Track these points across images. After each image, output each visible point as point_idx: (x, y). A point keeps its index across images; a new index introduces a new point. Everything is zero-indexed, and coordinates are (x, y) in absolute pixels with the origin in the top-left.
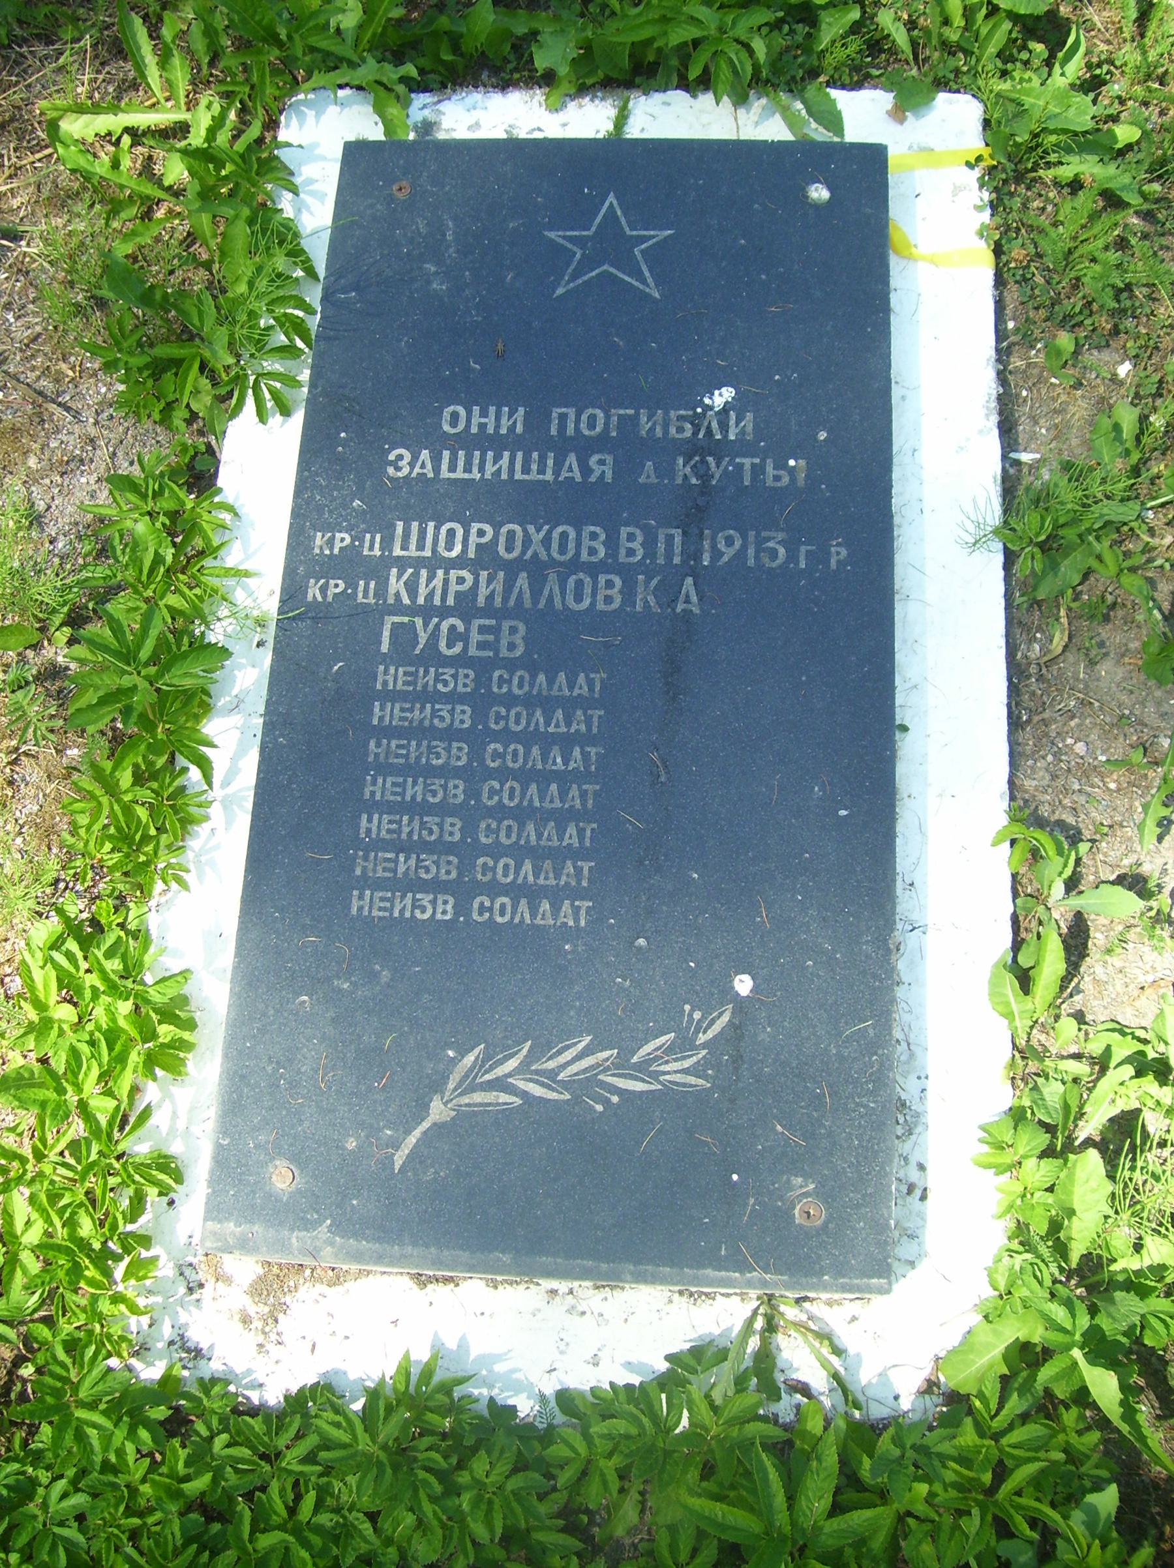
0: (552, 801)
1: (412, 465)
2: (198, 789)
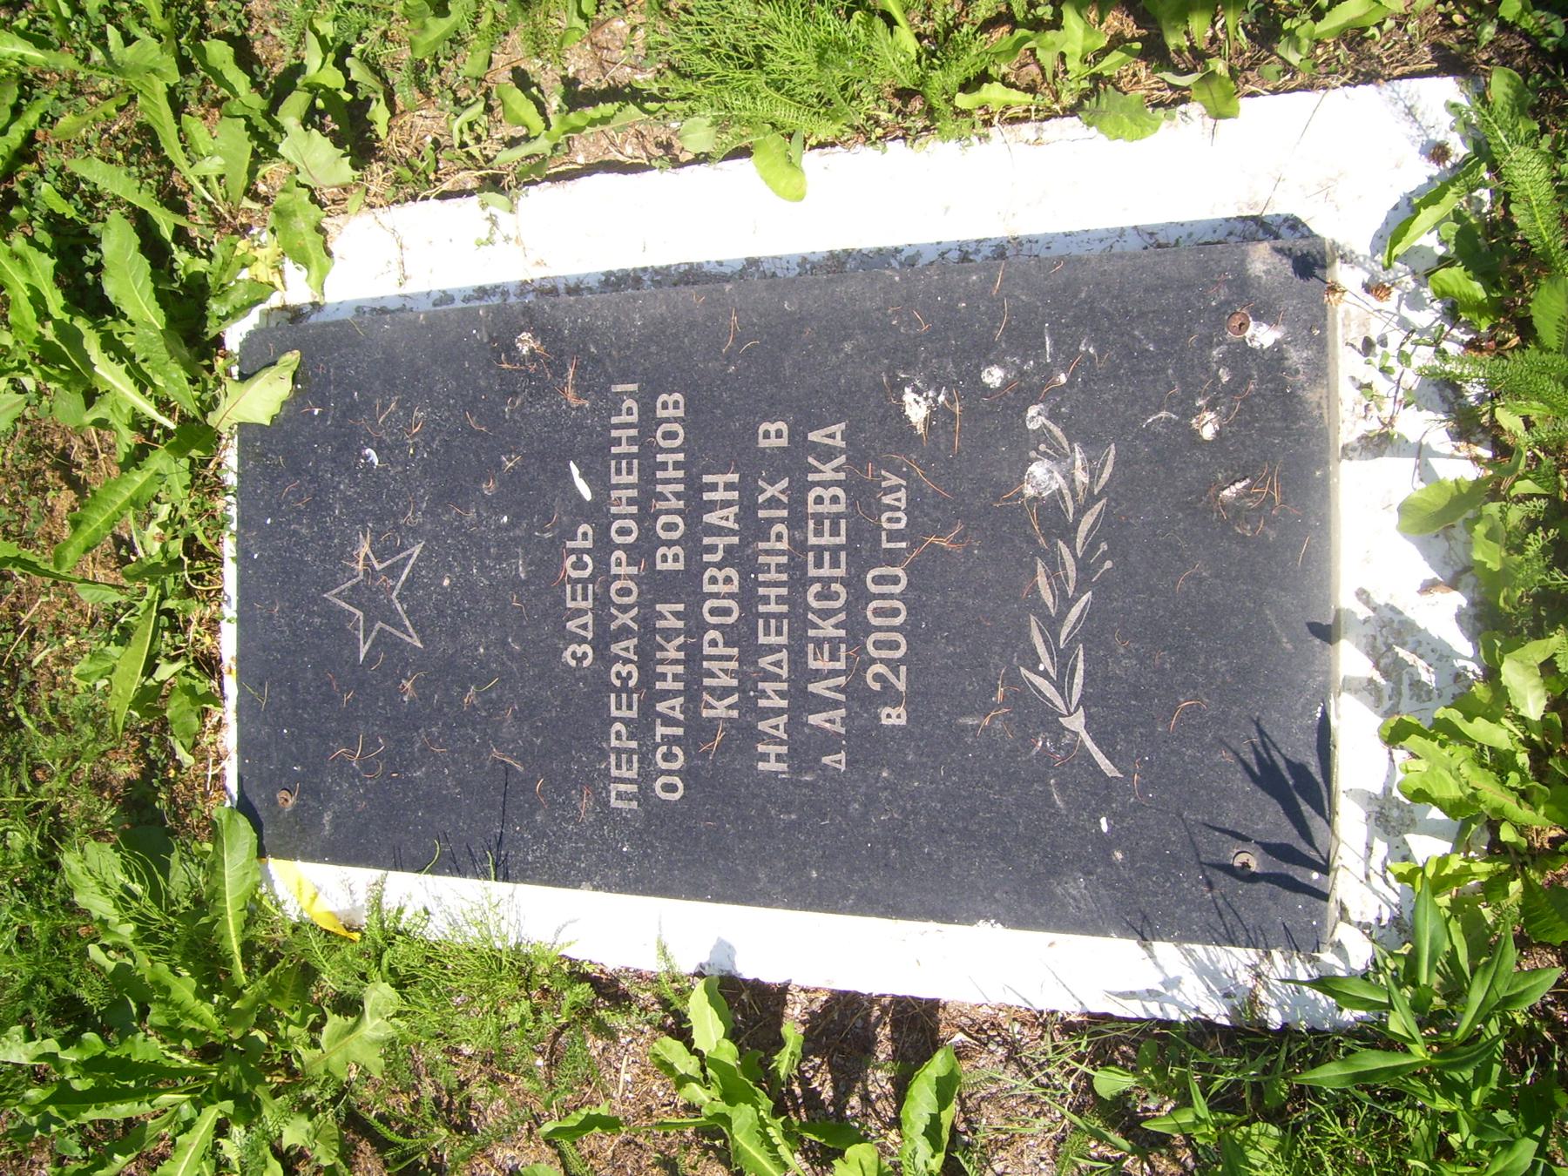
0: (899, 500)
1: (626, 661)
2: (362, 898)
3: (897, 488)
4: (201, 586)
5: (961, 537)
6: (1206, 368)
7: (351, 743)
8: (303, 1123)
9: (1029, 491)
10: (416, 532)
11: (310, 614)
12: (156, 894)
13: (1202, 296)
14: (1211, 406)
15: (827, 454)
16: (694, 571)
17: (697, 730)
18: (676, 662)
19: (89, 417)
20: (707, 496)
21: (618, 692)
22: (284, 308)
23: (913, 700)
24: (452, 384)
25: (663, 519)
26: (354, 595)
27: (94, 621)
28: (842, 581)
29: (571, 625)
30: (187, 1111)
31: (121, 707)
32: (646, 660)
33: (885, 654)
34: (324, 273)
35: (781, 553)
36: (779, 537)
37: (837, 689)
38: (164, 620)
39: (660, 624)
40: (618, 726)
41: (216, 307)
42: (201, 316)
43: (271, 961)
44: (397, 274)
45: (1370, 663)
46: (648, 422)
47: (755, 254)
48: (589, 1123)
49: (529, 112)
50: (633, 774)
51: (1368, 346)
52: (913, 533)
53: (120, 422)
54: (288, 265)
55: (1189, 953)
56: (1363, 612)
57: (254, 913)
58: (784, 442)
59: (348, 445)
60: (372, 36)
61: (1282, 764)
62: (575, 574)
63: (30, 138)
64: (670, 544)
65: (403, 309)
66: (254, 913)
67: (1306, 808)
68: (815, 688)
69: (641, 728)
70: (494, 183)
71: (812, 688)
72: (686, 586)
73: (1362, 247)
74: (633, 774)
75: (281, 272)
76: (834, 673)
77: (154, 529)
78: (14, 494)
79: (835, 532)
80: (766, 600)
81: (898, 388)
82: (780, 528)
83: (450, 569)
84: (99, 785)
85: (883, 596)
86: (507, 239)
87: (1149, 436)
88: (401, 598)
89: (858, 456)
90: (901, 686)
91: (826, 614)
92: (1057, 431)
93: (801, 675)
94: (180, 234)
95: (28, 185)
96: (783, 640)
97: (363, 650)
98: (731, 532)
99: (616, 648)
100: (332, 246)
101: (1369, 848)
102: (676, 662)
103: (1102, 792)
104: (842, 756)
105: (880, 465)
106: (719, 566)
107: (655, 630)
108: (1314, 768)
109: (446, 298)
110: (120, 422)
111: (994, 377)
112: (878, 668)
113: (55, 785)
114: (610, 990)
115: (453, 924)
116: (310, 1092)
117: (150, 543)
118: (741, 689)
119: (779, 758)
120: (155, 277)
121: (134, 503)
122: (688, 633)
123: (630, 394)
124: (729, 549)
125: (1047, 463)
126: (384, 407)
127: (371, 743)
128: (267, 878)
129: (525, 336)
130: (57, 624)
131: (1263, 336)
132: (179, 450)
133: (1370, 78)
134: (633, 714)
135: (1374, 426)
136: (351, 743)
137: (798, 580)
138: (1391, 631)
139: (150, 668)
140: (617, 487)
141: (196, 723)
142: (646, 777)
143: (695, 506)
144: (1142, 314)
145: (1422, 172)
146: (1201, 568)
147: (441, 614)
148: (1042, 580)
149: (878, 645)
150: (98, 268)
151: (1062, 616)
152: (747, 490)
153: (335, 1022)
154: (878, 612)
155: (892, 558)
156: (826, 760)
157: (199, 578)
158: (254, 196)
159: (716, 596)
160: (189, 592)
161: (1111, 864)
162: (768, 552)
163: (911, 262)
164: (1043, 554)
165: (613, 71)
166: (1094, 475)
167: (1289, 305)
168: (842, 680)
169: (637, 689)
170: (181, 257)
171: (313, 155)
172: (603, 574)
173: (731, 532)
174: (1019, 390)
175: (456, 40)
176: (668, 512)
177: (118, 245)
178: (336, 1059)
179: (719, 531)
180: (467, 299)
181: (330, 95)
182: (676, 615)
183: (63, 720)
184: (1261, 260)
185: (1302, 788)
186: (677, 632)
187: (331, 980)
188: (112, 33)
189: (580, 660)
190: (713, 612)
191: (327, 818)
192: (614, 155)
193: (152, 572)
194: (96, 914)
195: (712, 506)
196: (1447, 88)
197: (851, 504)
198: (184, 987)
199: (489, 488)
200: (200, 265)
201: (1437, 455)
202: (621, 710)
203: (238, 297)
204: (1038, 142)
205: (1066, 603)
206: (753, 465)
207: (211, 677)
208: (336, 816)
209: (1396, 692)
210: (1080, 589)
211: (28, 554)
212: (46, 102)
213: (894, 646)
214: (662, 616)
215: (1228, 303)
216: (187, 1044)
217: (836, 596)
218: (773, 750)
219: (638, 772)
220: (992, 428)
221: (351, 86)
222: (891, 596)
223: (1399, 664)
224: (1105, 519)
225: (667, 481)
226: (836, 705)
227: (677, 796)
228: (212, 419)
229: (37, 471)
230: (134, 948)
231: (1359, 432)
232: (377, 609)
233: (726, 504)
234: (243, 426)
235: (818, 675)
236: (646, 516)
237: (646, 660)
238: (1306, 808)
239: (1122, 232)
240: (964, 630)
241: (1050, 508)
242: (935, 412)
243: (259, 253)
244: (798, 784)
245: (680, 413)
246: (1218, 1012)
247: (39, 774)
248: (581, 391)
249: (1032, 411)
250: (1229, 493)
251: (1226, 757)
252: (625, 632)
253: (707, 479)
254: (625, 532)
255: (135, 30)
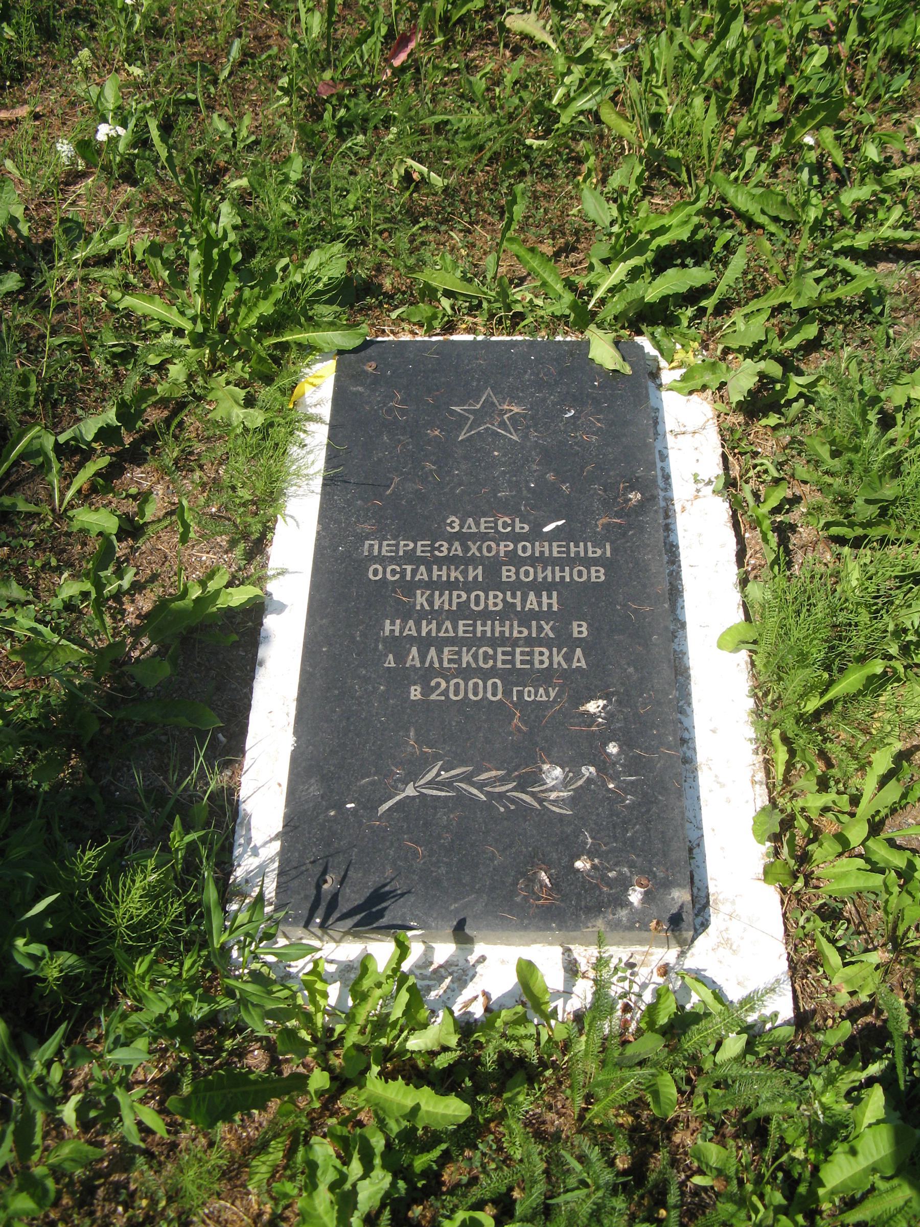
1: (449, 550)
3: (548, 695)
4: (495, 322)
5: (519, 730)
6: (616, 864)
7: (403, 402)
8: (182, 379)
9: (546, 767)
10: (525, 437)
11: (479, 380)
12: (318, 293)
13: (659, 863)
14: (594, 867)
15: (568, 658)
16: (501, 586)
17: (410, 588)
18: (449, 576)
19: (595, 261)
20: (544, 593)
21: (431, 546)
22: (659, 369)
23: (425, 705)
24: (611, 456)
25: (531, 570)
26: (489, 404)
27: (476, 266)
28: (494, 666)
29: (470, 520)
30: (190, 312)
31: (426, 276)
32: (450, 561)
33: (452, 689)
34: (679, 390)
35: (511, 633)
36: (520, 632)
37: (432, 662)
38: (476, 302)
39: (471, 568)
40: (412, 545)
41: (659, 330)
42: (653, 323)
43: (276, 360)
44: (677, 430)
45: (442, 962)
46: (588, 562)
47: (688, 626)
48: (186, 526)
49: (773, 502)
50: (384, 553)
51: (631, 966)
52: (521, 704)
53: (592, 277)
54: (683, 371)
55: (272, 860)
56: (472, 959)
57: (306, 349)
58: (575, 635)
59: (577, 400)
60: (820, 416)
61: (384, 905)
62: (500, 523)
63: (761, 226)
64: (517, 573)
65: (656, 434)
66: (306, 349)
67: (358, 917)
68: (433, 652)
69: (410, 557)
70: (731, 484)
71: (433, 649)
72: (492, 582)
73: (690, 963)
74: (384, 553)
75: (679, 367)
76: (441, 661)
77: (529, 296)
78: (550, 220)
79: (522, 662)
80: (484, 625)
81: (607, 697)
82: (526, 632)
83: (504, 455)
84: (379, 268)
85: (485, 687)
86: (698, 491)
87: (577, 833)
88: (487, 429)
89: (567, 675)
90: (433, 697)
91: (475, 657)
92: (580, 783)
93: (440, 643)
94: (702, 311)
95: (732, 226)
96: (461, 634)
97: (457, 409)
98: (523, 606)
99: (457, 544)
100: (694, 397)
101: (331, 962)
102: (449, 576)
103: (369, 804)
104: (393, 665)
105: (561, 686)
106: (504, 600)
107: (467, 565)
108: (383, 921)
109: (664, 457)
110: (592, 277)
111: (613, 749)
112: (444, 685)
113: (380, 243)
114: (258, 547)
115: (297, 460)
116: (200, 381)
117: (521, 295)
118: (432, 611)
119: (392, 631)
120: (676, 295)
121: (544, 284)
122: (466, 583)
123: (604, 553)
124: (514, 605)
125: (561, 777)
126: (599, 420)
127: (403, 412)
128: (325, 357)
129: (639, 496)
130: (473, 245)
131: (635, 896)
132: (573, 306)
133: (793, 967)
134: (419, 553)
135: (583, 967)
136: (403, 402)
137: (494, 642)
138: (461, 974)
139: (448, 294)
140: (550, 546)
141: (415, 320)
142: (381, 560)
143: (538, 587)
144: (649, 830)
145: (734, 994)
146: (499, 859)
147: (477, 451)
148: (494, 773)
149: (457, 685)
150: (684, 266)
151: (473, 784)
152: (548, 615)
153: (241, 394)
154: (476, 685)
155: (507, 693)
156: (391, 657)
157: (500, 322)
158: (726, 351)
159: (487, 598)
160: (492, 316)
161: (328, 809)
162: (511, 626)
163: (682, 711)
164: (509, 774)
165: (800, 552)
166: (555, 802)
167: (654, 910)
168: (437, 665)
169: (433, 555)
170: (690, 312)
171: (743, 378)
172: (500, 537)
173: (523, 606)
174: (604, 762)
175: (817, 463)
176: (535, 573)
177: (697, 276)
178: (219, 394)
179: (524, 600)
180: (663, 469)
181: (785, 390)
182: (476, 577)
183: (417, 249)
184: (680, 896)
185: (369, 917)
186: (466, 577)
187: (265, 393)
188: (822, 272)
189: (450, 525)
190: (477, 596)
191: (360, 389)
192: (749, 553)
193: (503, 294)
194: (307, 261)
195: (539, 596)
196: (787, 1012)
197: (539, 670)
198: (266, 308)
199: (551, 477)
200: (685, 323)
201: (565, 1003)
202: (421, 547)
203: (665, 342)
204: (754, 782)
205: (480, 786)
206: (562, 619)
207: (442, 329)
208: (361, 394)
209: (424, 977)
210: (487, 794)
211: (515, 226)
212: (782, 235)
213: (456, 693)
214: (475, 569)
215: (655, 876)
216: (230, 311)
217: (485, 662)
218: (397, 628)
219: (384, 556)
220: (583, 746)
221: (789, 403)
222: (485, 691)
223: (442, 979)
224: (529, 809)
225: (553, 572)
226: (423, 661)
227: (371, 576)
228: (592, 327)
229: (564, 234)
230: (287, 283)
231: (579, 959)
232: (480, 416)
233: (540, 604)
234: (588, 343)
235: (440, 652)
236: (533, 561)
237: (450, 561)
238: (358, 917)
239: (700, 828)
240: (463, 731)
241: (536, 778)
242: (592, 717)
243: (691, 354)
244: (377, 641)
245: (593, 579)
246: (239, 873)
247: (386, 234)
248: (607, 526)
249: (592, 769)
250: (543, 875)
251: (389, 872)
252: (466, 549)
253: (555, 594)
254: (525, 550)
255: (822, 284)
